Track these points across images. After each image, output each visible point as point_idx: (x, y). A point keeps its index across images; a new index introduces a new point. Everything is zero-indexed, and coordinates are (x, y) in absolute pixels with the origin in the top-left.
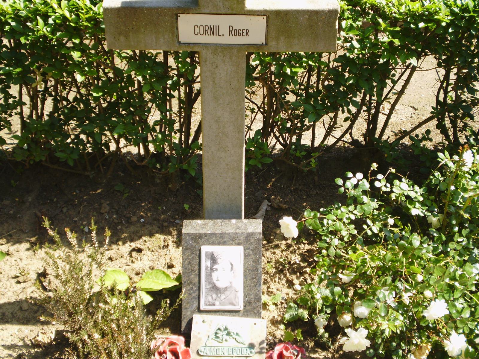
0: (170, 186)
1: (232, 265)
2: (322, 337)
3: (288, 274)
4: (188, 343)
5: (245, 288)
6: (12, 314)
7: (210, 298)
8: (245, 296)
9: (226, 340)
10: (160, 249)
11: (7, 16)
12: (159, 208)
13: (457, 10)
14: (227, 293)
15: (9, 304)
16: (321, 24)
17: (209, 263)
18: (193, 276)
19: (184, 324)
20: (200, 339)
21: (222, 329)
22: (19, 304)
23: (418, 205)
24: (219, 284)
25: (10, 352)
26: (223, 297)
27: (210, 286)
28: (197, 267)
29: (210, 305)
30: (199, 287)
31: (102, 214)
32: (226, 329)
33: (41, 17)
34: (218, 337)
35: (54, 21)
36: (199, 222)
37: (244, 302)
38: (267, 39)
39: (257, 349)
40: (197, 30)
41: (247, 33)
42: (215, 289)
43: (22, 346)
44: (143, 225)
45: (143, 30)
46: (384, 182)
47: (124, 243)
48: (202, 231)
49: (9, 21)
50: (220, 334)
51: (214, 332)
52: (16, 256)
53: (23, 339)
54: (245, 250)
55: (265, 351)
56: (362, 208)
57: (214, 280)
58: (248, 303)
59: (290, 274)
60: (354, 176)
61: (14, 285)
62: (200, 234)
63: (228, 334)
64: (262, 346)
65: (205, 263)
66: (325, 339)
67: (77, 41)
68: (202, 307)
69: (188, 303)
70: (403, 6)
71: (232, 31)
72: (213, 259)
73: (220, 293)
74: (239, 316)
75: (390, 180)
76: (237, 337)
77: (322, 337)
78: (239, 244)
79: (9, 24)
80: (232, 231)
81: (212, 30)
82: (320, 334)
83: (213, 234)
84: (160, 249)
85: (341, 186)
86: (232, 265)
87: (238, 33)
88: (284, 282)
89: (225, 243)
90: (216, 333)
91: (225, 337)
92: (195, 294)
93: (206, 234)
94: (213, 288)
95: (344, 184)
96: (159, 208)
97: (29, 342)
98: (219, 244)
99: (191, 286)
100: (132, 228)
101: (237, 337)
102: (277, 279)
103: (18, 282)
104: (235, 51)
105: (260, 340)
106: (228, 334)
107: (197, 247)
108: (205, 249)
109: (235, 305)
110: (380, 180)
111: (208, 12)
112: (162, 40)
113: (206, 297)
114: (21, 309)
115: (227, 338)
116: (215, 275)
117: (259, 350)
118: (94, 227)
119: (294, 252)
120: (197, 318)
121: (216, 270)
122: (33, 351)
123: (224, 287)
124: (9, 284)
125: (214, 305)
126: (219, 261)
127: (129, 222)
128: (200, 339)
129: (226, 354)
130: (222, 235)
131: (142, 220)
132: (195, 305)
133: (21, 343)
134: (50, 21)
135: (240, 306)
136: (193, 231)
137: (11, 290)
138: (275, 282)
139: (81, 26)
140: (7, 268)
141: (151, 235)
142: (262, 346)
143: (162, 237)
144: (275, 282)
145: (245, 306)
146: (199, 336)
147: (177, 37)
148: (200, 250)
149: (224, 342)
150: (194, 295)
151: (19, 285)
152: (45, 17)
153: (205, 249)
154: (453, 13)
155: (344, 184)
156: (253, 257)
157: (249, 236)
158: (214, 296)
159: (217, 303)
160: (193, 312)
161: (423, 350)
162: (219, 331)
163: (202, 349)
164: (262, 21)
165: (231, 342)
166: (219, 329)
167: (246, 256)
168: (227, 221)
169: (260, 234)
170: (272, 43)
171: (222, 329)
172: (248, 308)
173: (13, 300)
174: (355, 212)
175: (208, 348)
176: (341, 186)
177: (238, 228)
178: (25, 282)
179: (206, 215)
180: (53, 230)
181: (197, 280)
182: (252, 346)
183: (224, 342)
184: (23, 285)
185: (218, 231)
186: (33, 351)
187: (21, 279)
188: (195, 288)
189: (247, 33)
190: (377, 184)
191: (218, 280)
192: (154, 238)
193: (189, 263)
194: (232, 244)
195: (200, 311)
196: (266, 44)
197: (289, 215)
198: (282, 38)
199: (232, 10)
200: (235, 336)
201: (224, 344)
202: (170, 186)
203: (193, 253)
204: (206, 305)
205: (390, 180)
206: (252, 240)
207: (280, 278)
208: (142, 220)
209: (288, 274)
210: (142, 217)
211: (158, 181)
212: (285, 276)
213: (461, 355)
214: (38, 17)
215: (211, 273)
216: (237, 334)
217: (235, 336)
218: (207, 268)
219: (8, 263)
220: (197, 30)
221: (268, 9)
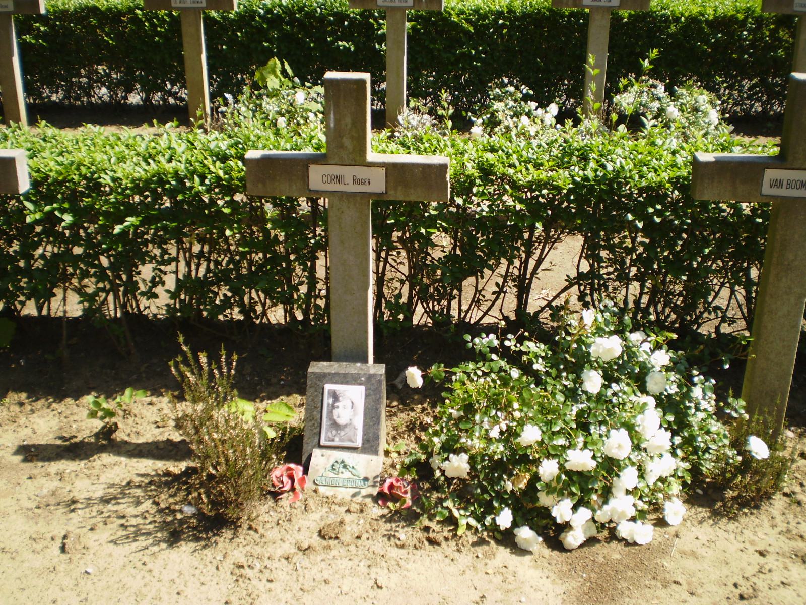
0: (313, 352)
1: (352, 403)
2: (438, 479)
3: (417, 431)
4: (306, 472)
5: (364, 426)
6: (148, 451)
7: (330, 434)
8: (364, 434)
9: (342, 473)
10: (295, 407)
11: (169, 176)
12: (301, 372)
13: (578, 180)
14: (347, 430)
15: (147, 443)
16: (433, 176)
17: (331, 401)
18: (315, 413)
19: (304, 459)
20: (318, 471)
21: (339, 462)
22: (156, 444)
23: (540, 360)
24: (341, 421)
25: (143, 479)
26: (342, 433)
27: (331, 423)
28: (319, 404)
29: (329, 441)
30: (321, 424)
31: (244, 375)
32: (343, 462)
33: (198, 176)
34: (334, 469)
35: (210, 181)
36: (325, 363)
37: (363, 440)
38: (386, 188)
39: (370, 483)
40: (325, 179)
41: (369, 182)
42: (335, 425)
43: (154, 476)
44: (283, 386)
45: (278, 178)
46: (513, 343)
47: (262, 401)
48: (327, 371)
49: (170, 180)
50: (337, 466)
51: (331, 464)
52: (159, 406)
53: (156, 471)
54: (366, 390)
55: (378, 484)
56: (489, 365)
57: (335, 418)
58: (366, 441)
59: (419, 431)
60: (487, 336)
61: (153, 429)
62: (324, 373)
63: (345, 467)
64: (376, 480)
65: (328, 401)
66: (441, 482)
67: (228, 199)
68: (323, 442)
69: (309, 438)
70: (531, 176)
71: (355, 180)
72: (335, 396)
73: (340, 430)
74: (357, 452)
75: (520, 340)
76: (353, 471)
77: (438, 479)
78: (360, 384)
79: (169, 183)
80: (356, 371)
81: (338, 179)
82: (436, 478)
83: (336, 374)
84: (295, 407)
85: (469, 342)
86: (352, 403)
87: (361, 182)
88: (413, 438)
89: (347, 383)
90: (333, 465)
91: (341, 469)
92: (318, 429)
93: (330, 374)
94: (333, 424)
95: (472, 340)
96: (301, 372)
97: (161, 473)
98: (342, 383)
99: (313, 422)
100: (271, 389)
101: (353, 471)
102: (406, 436)
103: (158, 427)
104: (358, 198)
105: (374, 475)
106: (345, 467)
107: (321, 385)
108: (328, 387)
109: (353, 442)
110: (510, 340)
111: (334, 163)
112: (294, 187)
113: (326, 433)
114: (157, 447)
115: (344, 470)
116: (336, 412)
117: (372, 484)
118: (223, 352)
119: (427, 415)
120: (317, 452)
121: (338, 407)
122: (163, 479)
123: (345, 423)
124: (148, 428)
125: (333, 440)
126: (340, 399)
127: (269, 384)
128: (318, 471)
129: (341, 485)
130: (345, 375)
131: (282, 382)
132: (316, 440)
133: (153, 473)
134: (207, 182)
135: (359, 443)
136: (318, 370)
137: (150, 433)
138: (404, 438)
139: (233, 185)
140: (148, 415)
141: (288, 394)
142: (376, 480)
143: (299, 398)
144: (404, 438)
145: (363, 444)
146: (317, 468)
147: (308, 185)
148: (323, 389)
149: (340, 474)
150: (315, 431)
151: (158, 430)
152: (203, 178)
153: (328, 387)
154: (574, 182)
155: (472, 340)
156: (373, 397)
157: (370, 377)
158: (334, 432)
159: (337, 439)
160: (314, 447)
161: (521, 479)
162: (336, 464)
163: (319, 479)
164: (382, 172)
165: (347, 475)
166: (337, 462)
167: (367, 396)
168: (352, 364)
169: (381, 375)
170: (392, 192)
171: (339, 462)
172: (365, 446)
173: (150, 441)
174: (483, 368)
175: (323, 479)
176: (469, 342)
177: (362, 369)
178: (164, 427)
179: (333, 358)
180: (187, 346)
181: (319, 416)
182: (366, 479)
183: (340, 474)
184: (161, 429)
185: (342, 371)
186: (163, 479)
187: (160, 424)
188: (316, 425)
189: (369, 182)
190: (507, 343)
191: (338, 417)
192: (291, 398)
193: (313, 400)
194: (354, 384)
195: (320, 446)
196: (386, 193)
197: (413, 365)
198: (400, 188)
199: (355, 161)
200: (350, 469)
201: (340, 476)
202: (313, 352)
203: (316, 391)
204: (326, 440)
205: (520, 340)
206: (373, 381)
207: (409, 435)
208: (282, 382)
209: (417, 431)
210: (282, 380)
211: (302, 347)
212: (414, 433)
213: (553, 480)
214: (195, 176)
215: (332, 410)
216: (353, 468)
217: (350, 469)
218: (329, 404)
219: (150, 411)
220: (325, 179)
221: (386, 161)
